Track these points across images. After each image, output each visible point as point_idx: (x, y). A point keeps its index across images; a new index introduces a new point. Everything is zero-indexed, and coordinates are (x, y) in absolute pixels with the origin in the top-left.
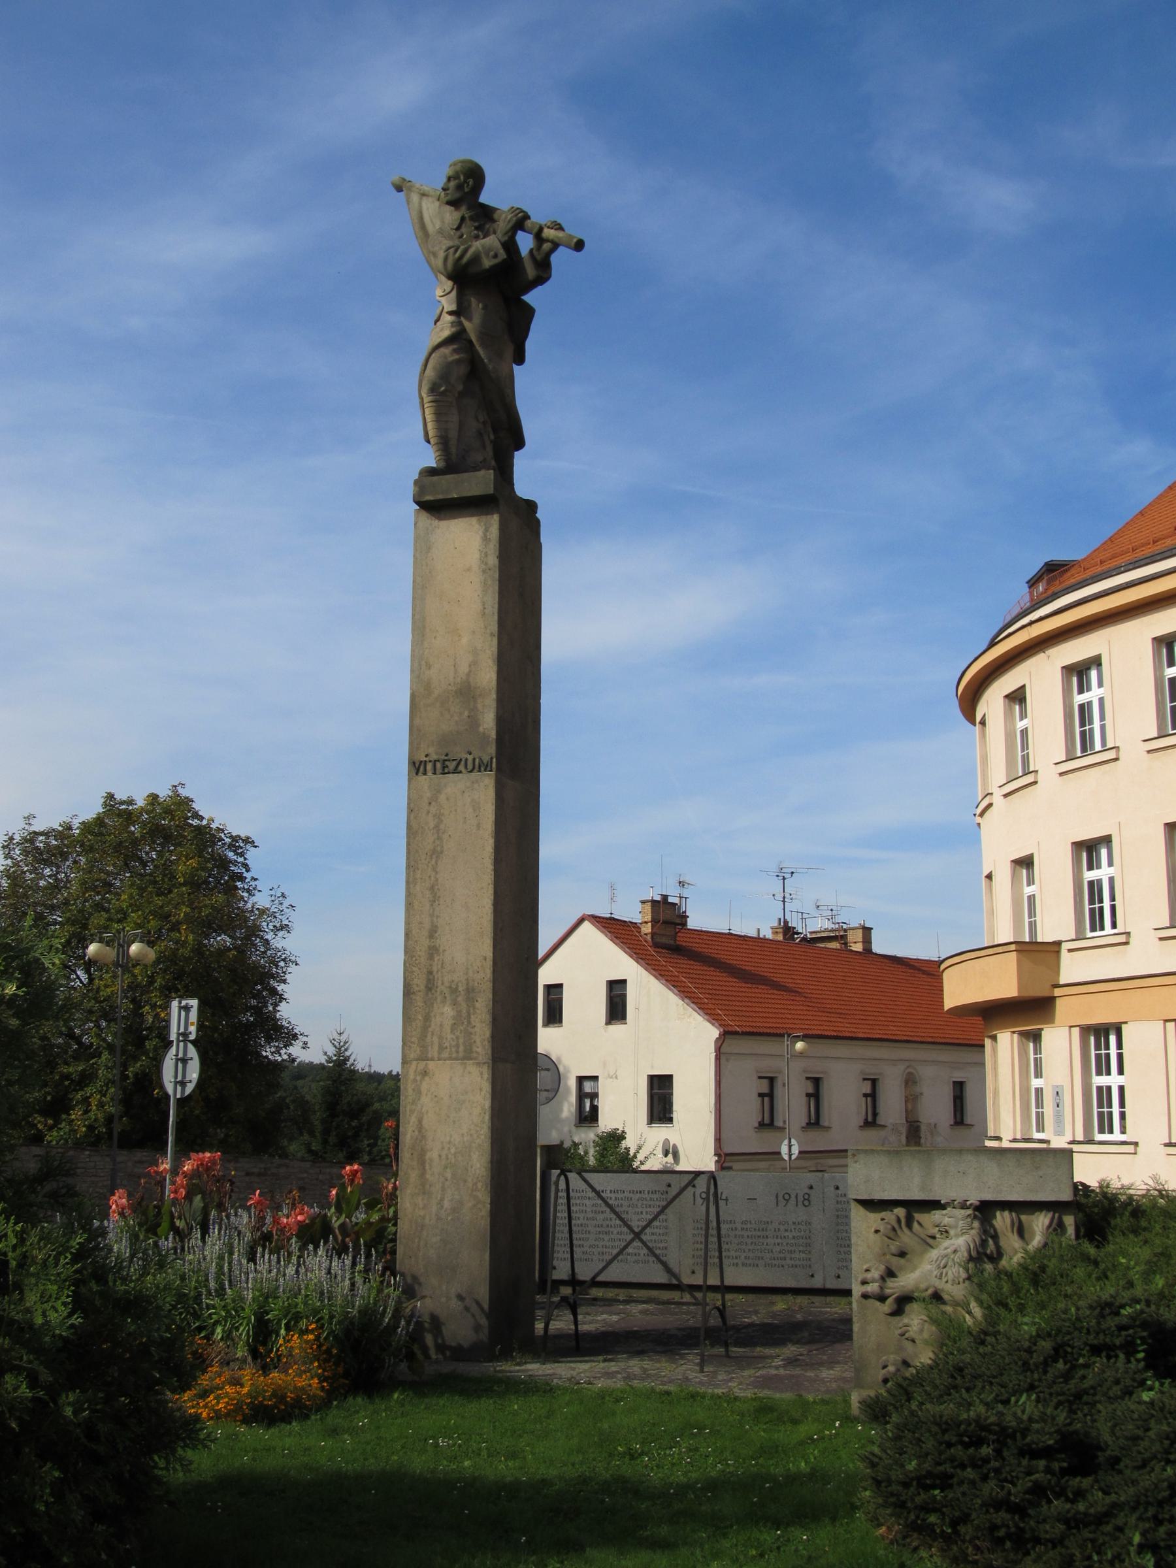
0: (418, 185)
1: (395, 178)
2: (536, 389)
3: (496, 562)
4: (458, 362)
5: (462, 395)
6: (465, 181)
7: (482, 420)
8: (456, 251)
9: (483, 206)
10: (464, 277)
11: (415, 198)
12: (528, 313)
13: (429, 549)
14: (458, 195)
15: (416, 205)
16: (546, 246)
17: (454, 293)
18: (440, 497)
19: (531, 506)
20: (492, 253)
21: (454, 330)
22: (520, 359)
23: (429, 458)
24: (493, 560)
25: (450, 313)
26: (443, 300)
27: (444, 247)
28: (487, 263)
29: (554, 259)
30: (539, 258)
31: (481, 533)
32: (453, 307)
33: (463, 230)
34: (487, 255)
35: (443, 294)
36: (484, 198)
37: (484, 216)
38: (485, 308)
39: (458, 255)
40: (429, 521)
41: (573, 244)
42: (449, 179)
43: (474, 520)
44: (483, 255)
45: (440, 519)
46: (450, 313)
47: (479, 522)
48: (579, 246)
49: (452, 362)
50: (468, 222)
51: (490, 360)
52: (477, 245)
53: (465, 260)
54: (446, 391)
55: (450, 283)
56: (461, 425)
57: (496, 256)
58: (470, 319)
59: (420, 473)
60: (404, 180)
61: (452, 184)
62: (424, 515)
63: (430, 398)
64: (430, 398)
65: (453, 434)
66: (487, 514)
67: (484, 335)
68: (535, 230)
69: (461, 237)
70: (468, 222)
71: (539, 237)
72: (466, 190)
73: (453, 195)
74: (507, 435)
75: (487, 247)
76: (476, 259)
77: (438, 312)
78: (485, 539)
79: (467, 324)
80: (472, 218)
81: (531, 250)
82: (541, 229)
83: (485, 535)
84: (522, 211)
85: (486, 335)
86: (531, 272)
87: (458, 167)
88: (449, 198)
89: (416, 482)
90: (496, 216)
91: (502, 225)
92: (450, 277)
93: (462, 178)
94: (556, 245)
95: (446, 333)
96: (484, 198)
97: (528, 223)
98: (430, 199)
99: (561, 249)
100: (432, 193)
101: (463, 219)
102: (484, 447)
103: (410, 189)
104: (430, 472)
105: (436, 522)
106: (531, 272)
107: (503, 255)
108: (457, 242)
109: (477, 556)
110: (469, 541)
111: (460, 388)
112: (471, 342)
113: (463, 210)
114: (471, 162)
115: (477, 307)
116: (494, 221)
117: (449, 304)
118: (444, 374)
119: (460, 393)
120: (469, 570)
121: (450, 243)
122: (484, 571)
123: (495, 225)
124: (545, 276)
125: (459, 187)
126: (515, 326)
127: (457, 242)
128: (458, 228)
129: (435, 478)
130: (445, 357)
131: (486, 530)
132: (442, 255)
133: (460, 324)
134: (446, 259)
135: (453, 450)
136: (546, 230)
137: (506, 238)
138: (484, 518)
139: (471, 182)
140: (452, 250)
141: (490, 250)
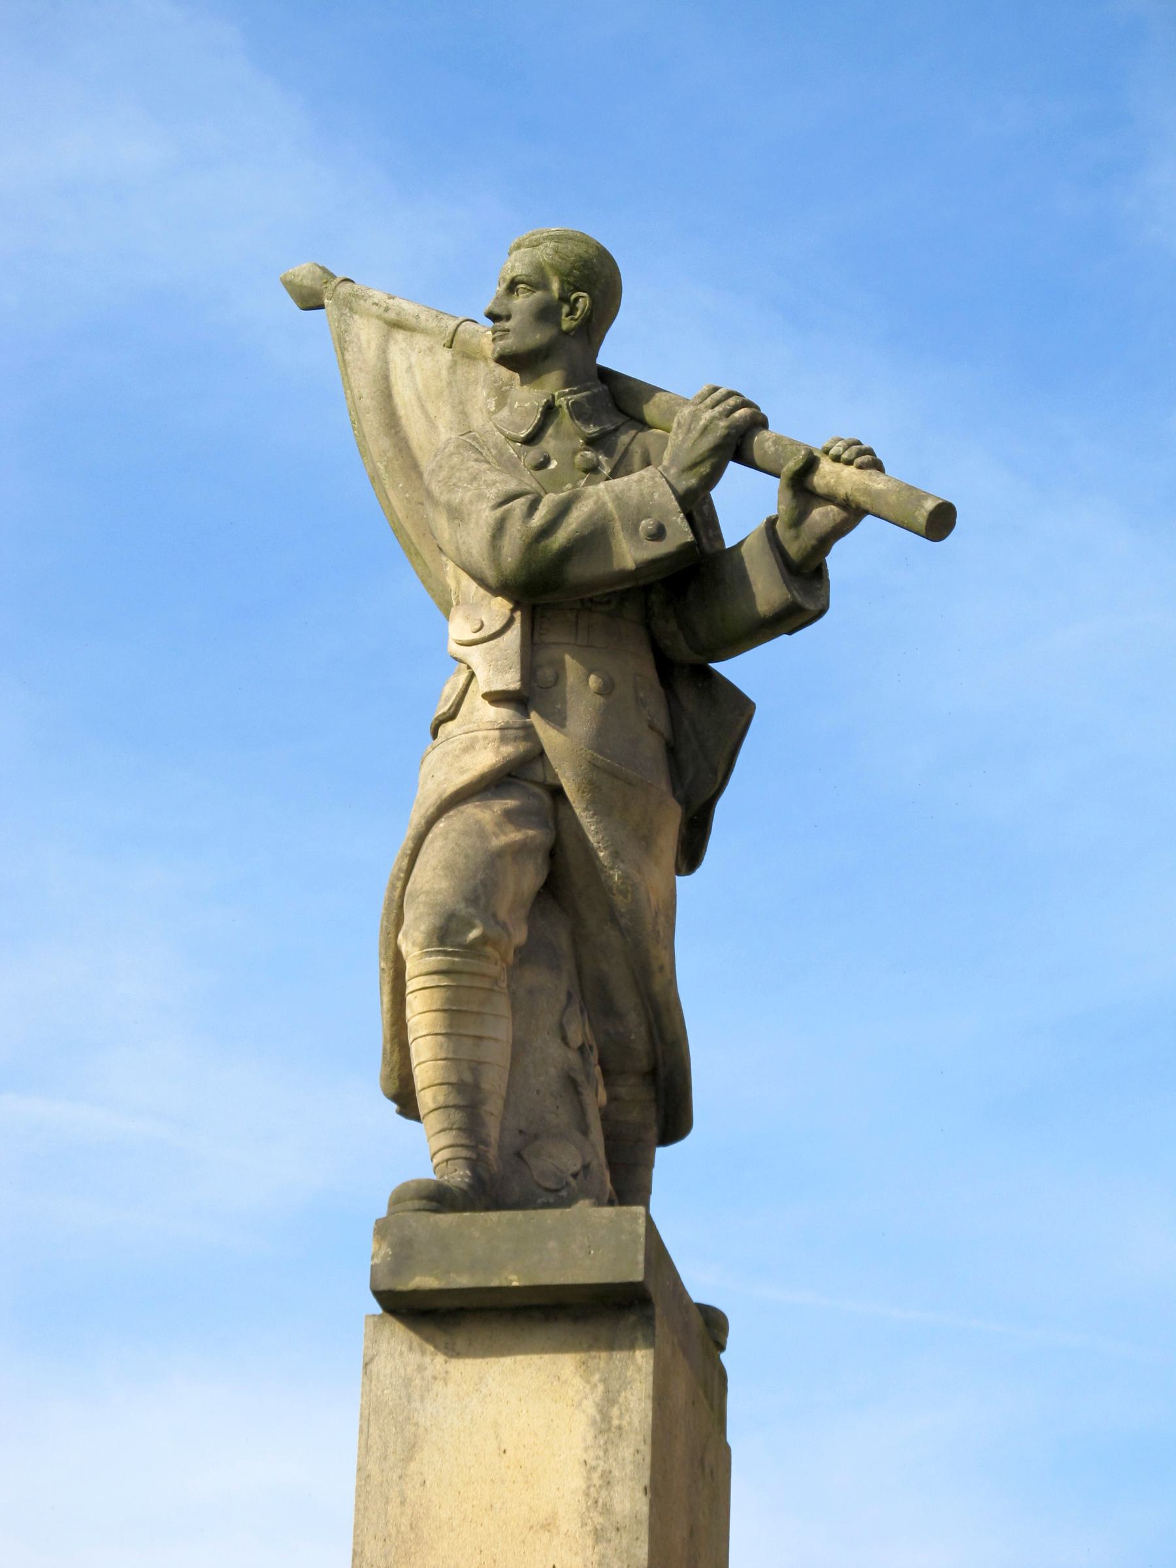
0: (378, 296)
1: (303, 271)
2: (732, 944)
3: (642, 1506)
4: (518, 851)
5: (525, 956)
6: (564, 299)
7: (576, 1038)
8: (533, 507)
9: (606, 375)
10: (547, 591)
11: (366, 332)
12: (736, 711)
13: (411, 1449)
14: (538, 337)
15: (371, 354)
16: (822, 516)
17: (514, 635)
18: (463, 1281)
19: (712, 1326)
20: (647, 525)
21: (508, 750)
22: (690, 855)
23: (420, 1151)
24: (631, 1501)
25: (496, 698)
26: (475, 657)
27: (493, 494)
28: (629, 553)
29: (838, 560)
30: (794, 549)
31: (590, 1407)
32: (510, 680)
33: (549, 443)
34: (633, 529)
35: (480, 643)
36: (613, 354)
37: (616, 408)
38: (606, 690)
39: (539, 518)
40: (414, 1358)
41: (922, 517)
42: (512, 287)
43: (566, 1364)
44: (618, 526)
45: (452, 1352)
46: (496, 698)
47: (586, 1370)
48: (941, 522)
49: (500, 854)
50: (565, 419)
51: (615, 855)
52: (600, 495)
53: (561, 537)
54: (483, 940)
55: (500, 607)
56: (519, 1049)
57: (659, 534)
58: (558, 719)
59: (398, 1199)
60: (329, 275)
61: (522, 302)
62: (398, 1335)
63: (434, 962)
64: (434, 962)
65: (495, 1081)
66: (611, 1347)
67: (605, 779)
68: (792, 465)
69: (543, 464)
70: (565, 419)
71: (801, 483)
72: (567, 323)
73: (524, 334)
74: (646, 1091)
75: (629, 507)
76: (595, 538)
77: (450, 691)
78: (605, 1427)
79: (547, 734)
80: (577, 412)
81: (771, 523)
82: (810, 464)
83: (605, 1417)
84: (746, 404)
85: (608, 778)
86: (767, 590)
87: (545, 253)
88: (509, 343)
89: (382, 1229)
90: (651, 411)
91: (679, 439)
92: (502, 589)
93: (555, 286)
94: (853, 512)
95: (485, 758)
96: (613, 354)
97: (763, 443)
98: (421, 341)
99: (868, 519)
100: (426, 319)
101: (550, 411)
102: (585, 1131)
103: (349, 305)
104: (439, 1198)
105: (437, 1362)
106: (767, 590)
107: (680, 533)
108: (529, 481)
109: (577, 1482)
110: (546, 1426)
111: (520, 935)
112: (557, 793)
113: (554, 383)
114: (585, 240)
115: (581, 684)
116: (643, 424)
117: (498, 667)
118: (480, 889)
119: (518, 950)
120: (548, 1526)
121: (512, 486)
122: (598, 1535)
123: (649, 437)
124: (811, 607)
125: (546, 314)
126: (691, 749)
127: (529, 481)
128: (531, 440)
129: (447, 1220)
130: (482, 834)
131: (609, 1399)
132: (486, 515)
133: (529, 732)
134: (499, 529)
135: (493, 1131)
136: (826, 466)
137: (692, 481)
138: (601, 1359)
139: (584, 302)
140: (519, 505)
141: (641, 512)
